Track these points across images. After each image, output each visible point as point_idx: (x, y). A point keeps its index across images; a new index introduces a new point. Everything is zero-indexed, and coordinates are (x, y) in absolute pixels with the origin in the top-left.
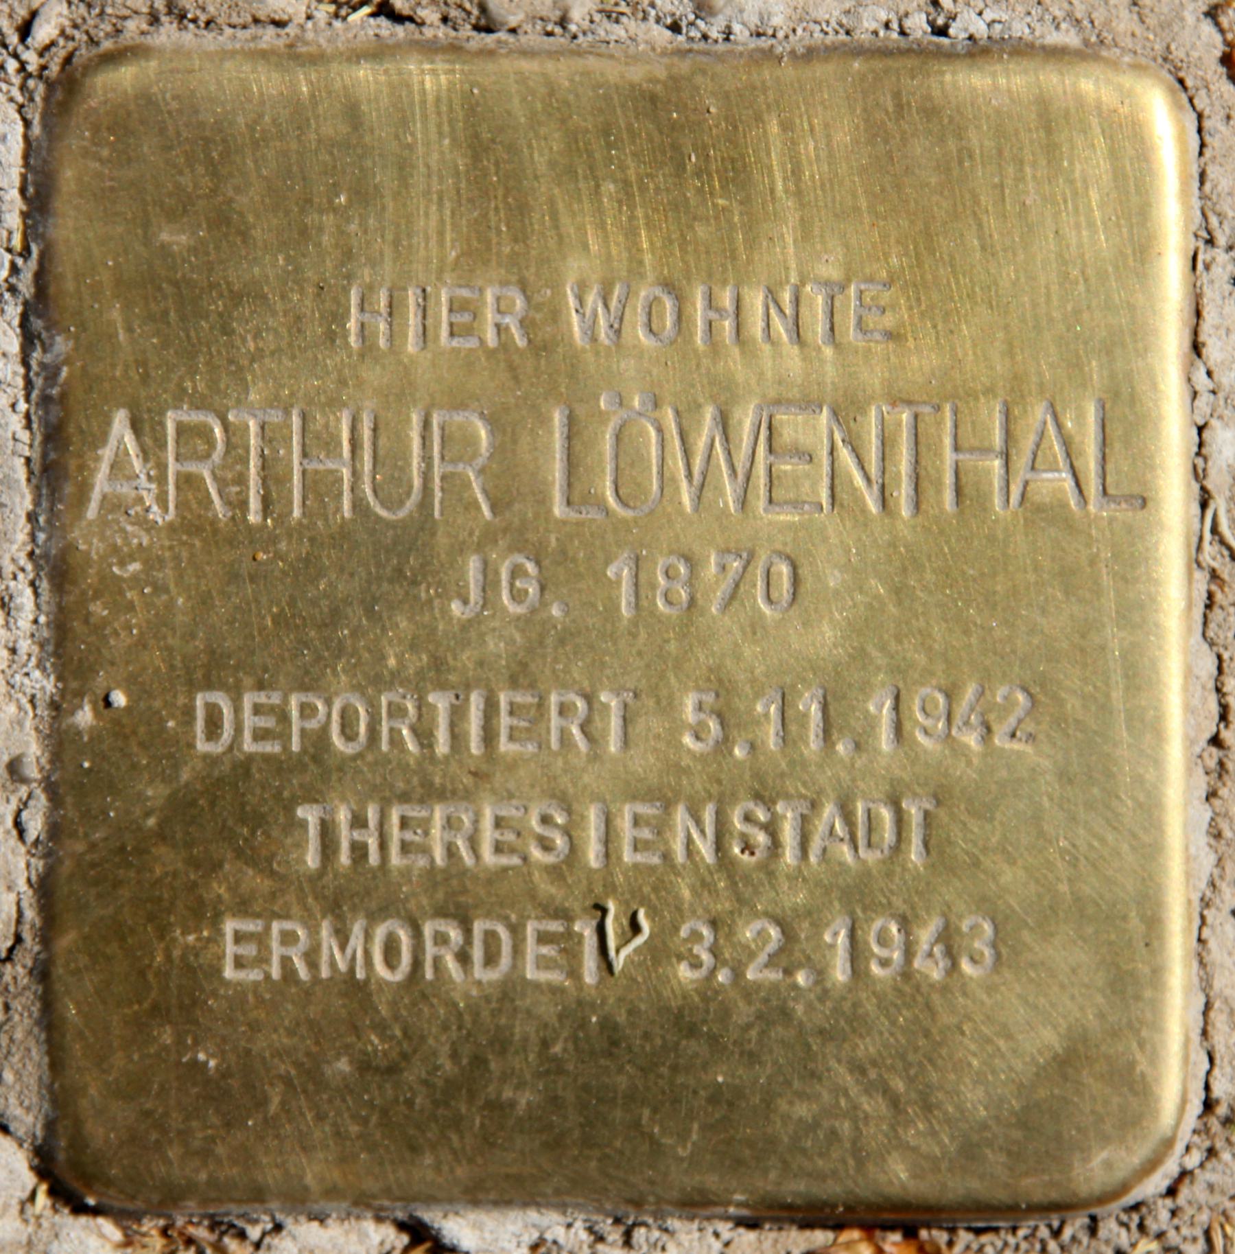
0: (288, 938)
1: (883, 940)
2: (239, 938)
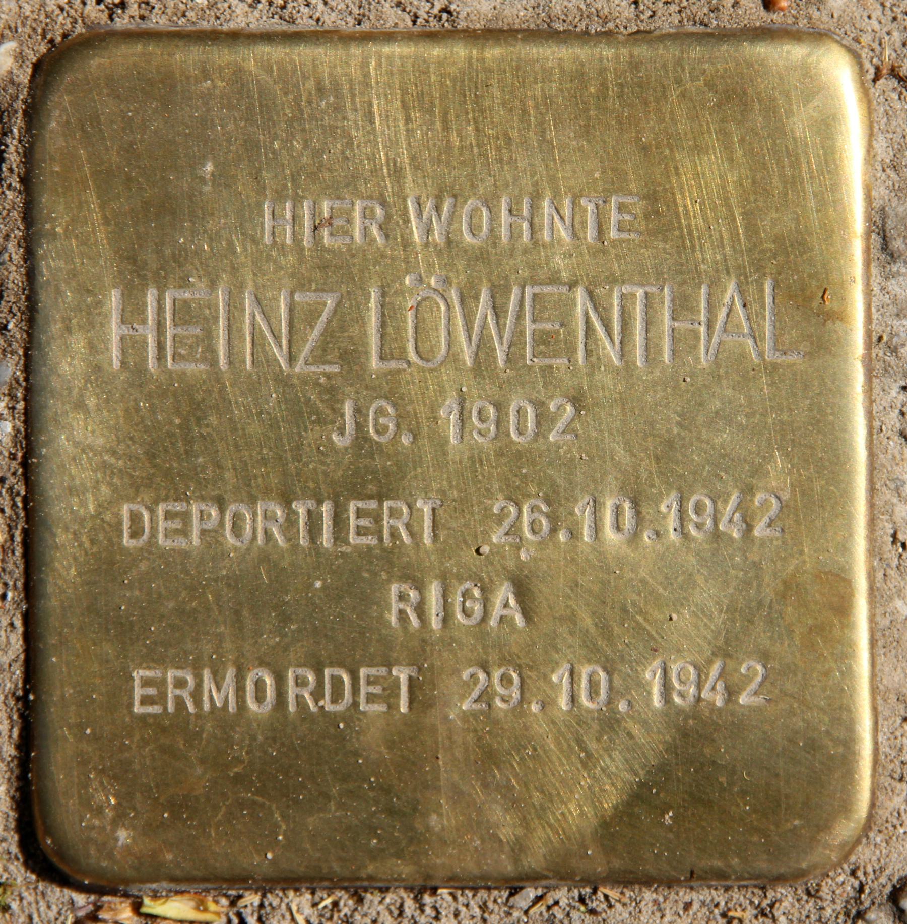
0: (180, 683)
2: (146, 683)
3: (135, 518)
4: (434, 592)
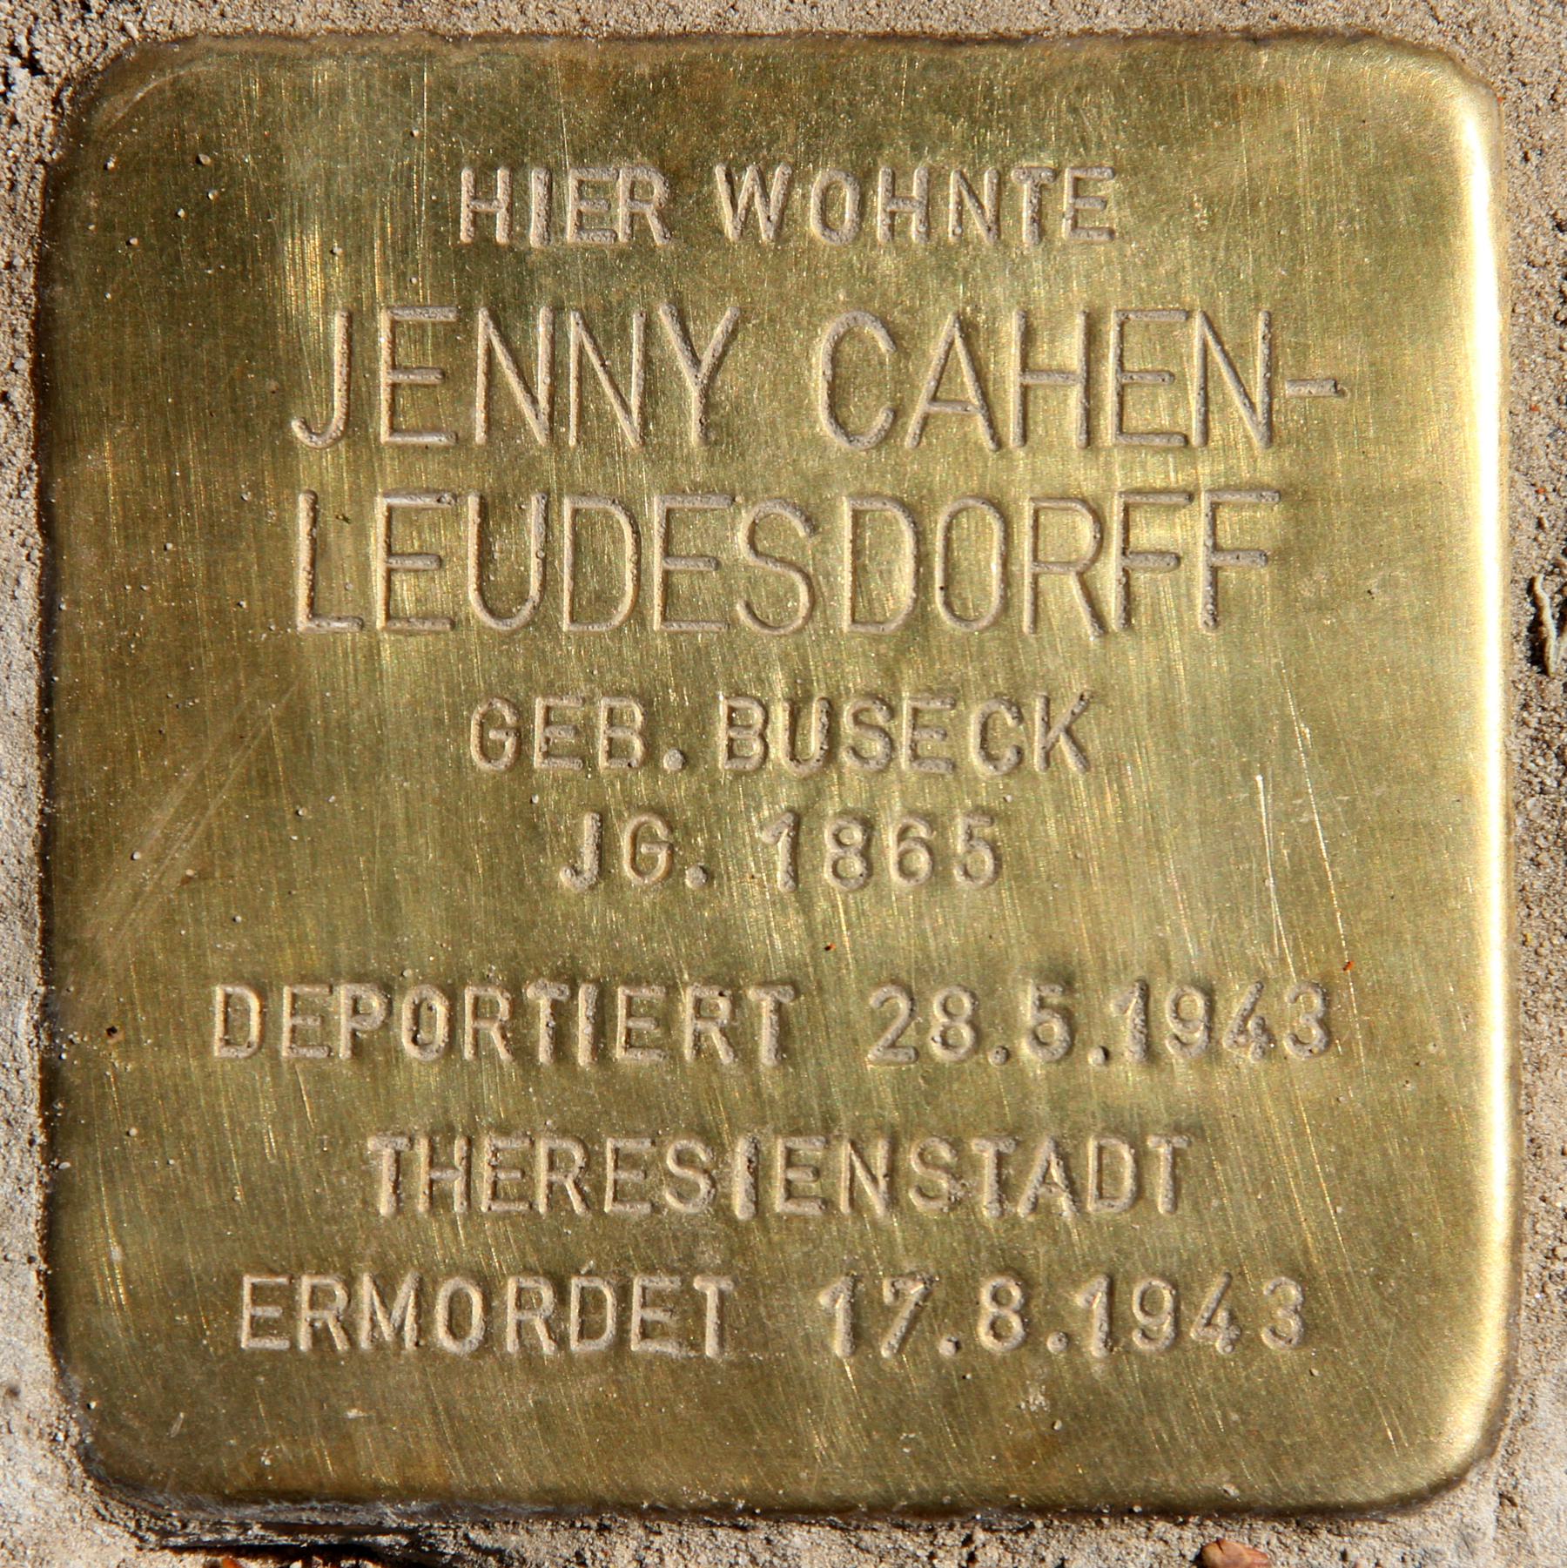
1: (1149, 1303)
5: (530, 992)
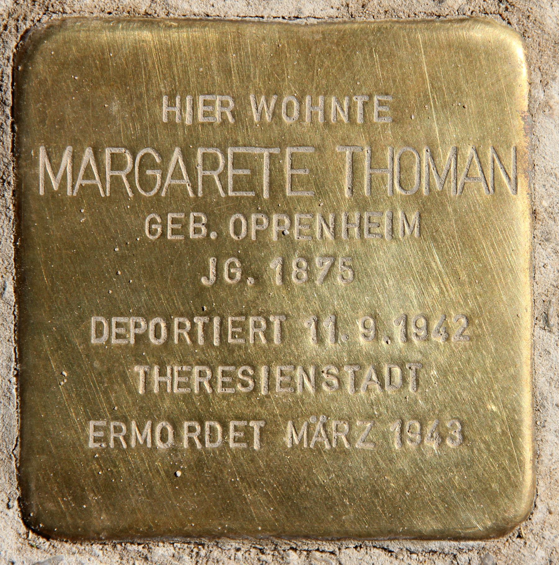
0: (118, 430)
3: (99, 325)
4: (263, 372)
5: (195, 320)
